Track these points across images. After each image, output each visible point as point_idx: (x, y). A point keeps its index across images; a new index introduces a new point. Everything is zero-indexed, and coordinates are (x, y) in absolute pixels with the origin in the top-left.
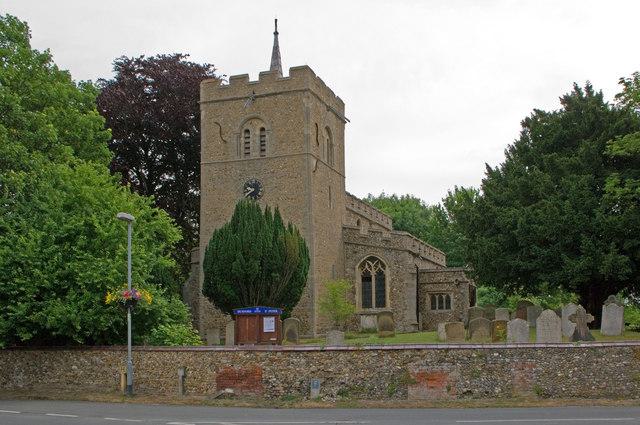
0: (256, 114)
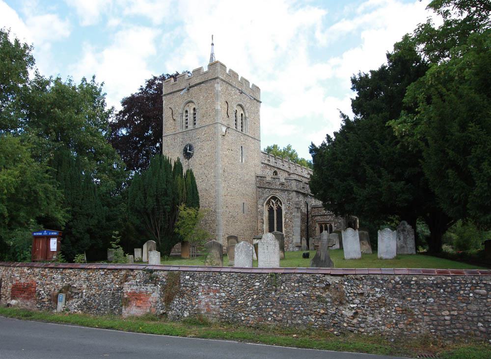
0: (189, 99)
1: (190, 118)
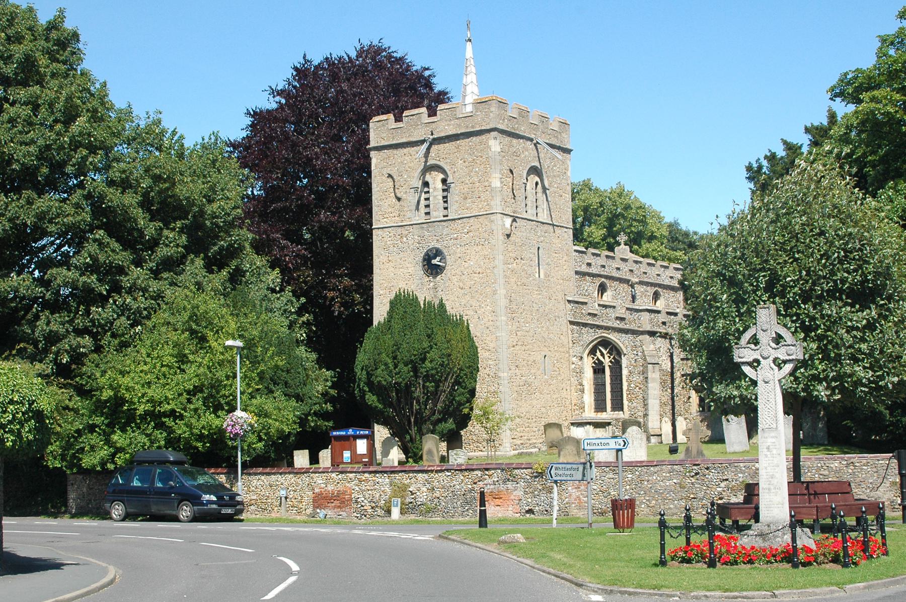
1: (435, 197)
